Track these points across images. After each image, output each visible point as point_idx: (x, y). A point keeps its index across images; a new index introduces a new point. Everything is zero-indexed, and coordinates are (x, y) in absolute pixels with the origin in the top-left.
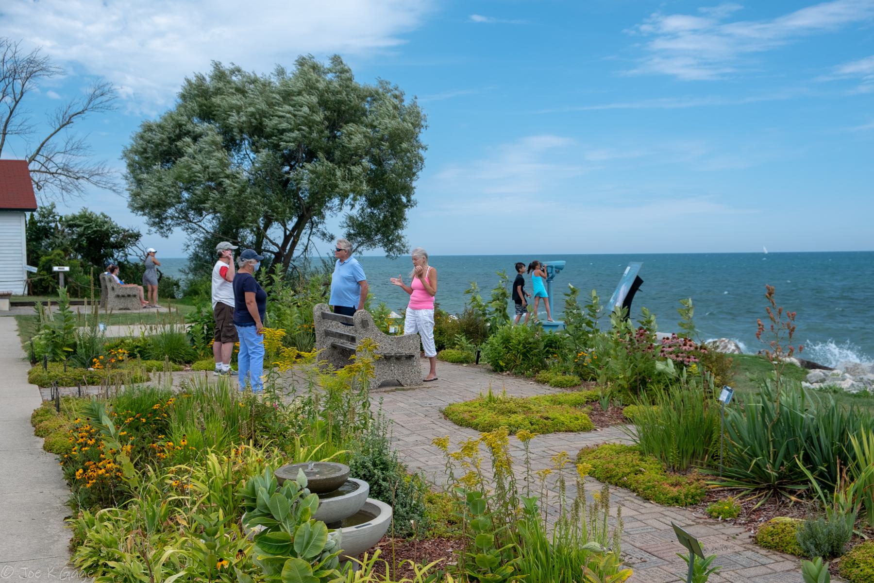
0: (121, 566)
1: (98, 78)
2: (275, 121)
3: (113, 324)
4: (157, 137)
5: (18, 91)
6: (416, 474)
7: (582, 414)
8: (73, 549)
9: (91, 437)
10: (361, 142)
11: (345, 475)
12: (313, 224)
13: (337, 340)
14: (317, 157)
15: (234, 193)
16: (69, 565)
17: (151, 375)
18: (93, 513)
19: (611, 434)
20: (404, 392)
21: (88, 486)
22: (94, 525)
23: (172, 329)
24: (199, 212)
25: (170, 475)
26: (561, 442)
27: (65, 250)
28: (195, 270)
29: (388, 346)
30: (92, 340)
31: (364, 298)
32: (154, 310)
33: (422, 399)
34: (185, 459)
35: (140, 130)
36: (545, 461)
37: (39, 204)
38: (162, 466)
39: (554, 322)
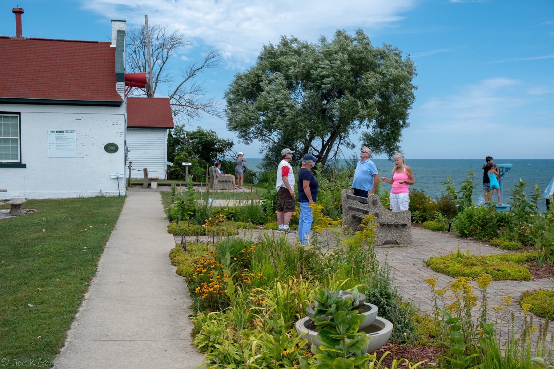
0: (222, 348)
1: (211, 47)
2: (319, 70)
3: (217, 199)
4: (244, 83)
5: (165, 56)
6: (409, 303)
7: (524, 269)
8: (194, 335)
9: (204, 267)
10: (375, 82)
11: (363, 301)
12: (341, 137)
13: (356, 213)
14: (344, 95)
15: (291, 117)
16: (192, 345)
17: (240, 231)
18: (206, 315)
19: (545, 283)
20: (400, 248)
21: (203, 297)
22: (206, 322)
23: (252, 202)
24: (270, 129)
25: (252, 294)
26: (508, 287)
27: (190, 153)
28: (266, 166)
29: (390, 218)
30: (205, 208)
31: (376, 186)
32: (242, 191)
33: (412, 253)
34: (261, 285)
35: (234, 79)
36: (496, 299)
37: (175, 124)
38: (246, 288)
39: (503, 205)
